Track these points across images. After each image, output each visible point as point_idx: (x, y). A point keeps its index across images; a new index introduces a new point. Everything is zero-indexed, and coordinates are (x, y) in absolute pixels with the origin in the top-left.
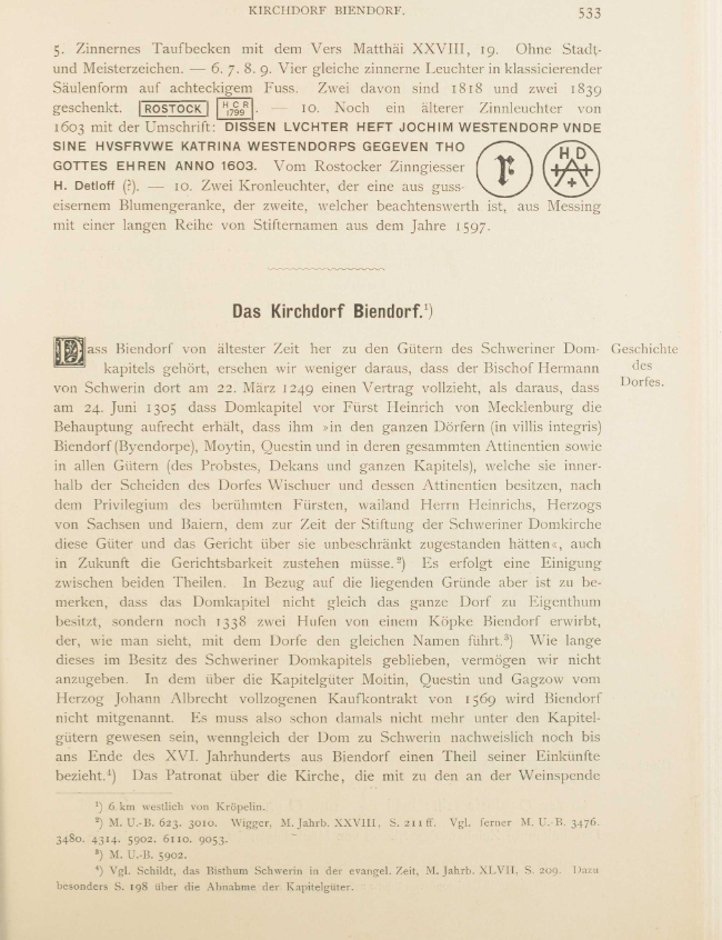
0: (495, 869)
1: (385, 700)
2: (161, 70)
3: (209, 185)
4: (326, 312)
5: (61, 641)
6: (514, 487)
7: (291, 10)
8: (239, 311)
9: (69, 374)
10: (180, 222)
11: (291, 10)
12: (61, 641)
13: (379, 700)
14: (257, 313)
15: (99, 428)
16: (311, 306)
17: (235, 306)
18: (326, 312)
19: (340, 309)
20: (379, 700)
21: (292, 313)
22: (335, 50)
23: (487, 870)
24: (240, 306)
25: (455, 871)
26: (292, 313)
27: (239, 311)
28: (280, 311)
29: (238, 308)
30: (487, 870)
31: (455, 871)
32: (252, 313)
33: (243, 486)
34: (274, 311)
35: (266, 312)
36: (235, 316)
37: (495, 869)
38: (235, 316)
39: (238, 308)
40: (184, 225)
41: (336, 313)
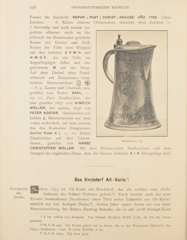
0: (126, 217)
1: (53, 199)
2: (42, 189)
3: (49, 98)
4: (98, 180)
5: (31, 128)
6: (133, 195)
7: (92, 7)
8: (76, 180)
9: (35, 195)
10: (50, 127)
11: (92, 7)
12: (31, 128)
13: (50, 199)
14: (81, 180)
15: (158, 210)
16: (95, 178)
17: (75, 178)
18: (98, 180)
19: (102, 179)
20: (50, 199)
21: (90, 180)
22: (89, 129)
23: (124, 217)
24: (77, 178)
25: (116, 217)
26: (90, 180)
27: (76, 180)
28: (87, 180)
29: (76, 179)
30: (124, 217)
31: (116, 217)
32: (80, 180)
33: (20, 198)
34: (85, 180)
35: (83, 180)
36: (75, 181)
37: (126, 217)
38: (75, 181)
39: (76, 179)
40: (56, 38)
41: (101, 180)
